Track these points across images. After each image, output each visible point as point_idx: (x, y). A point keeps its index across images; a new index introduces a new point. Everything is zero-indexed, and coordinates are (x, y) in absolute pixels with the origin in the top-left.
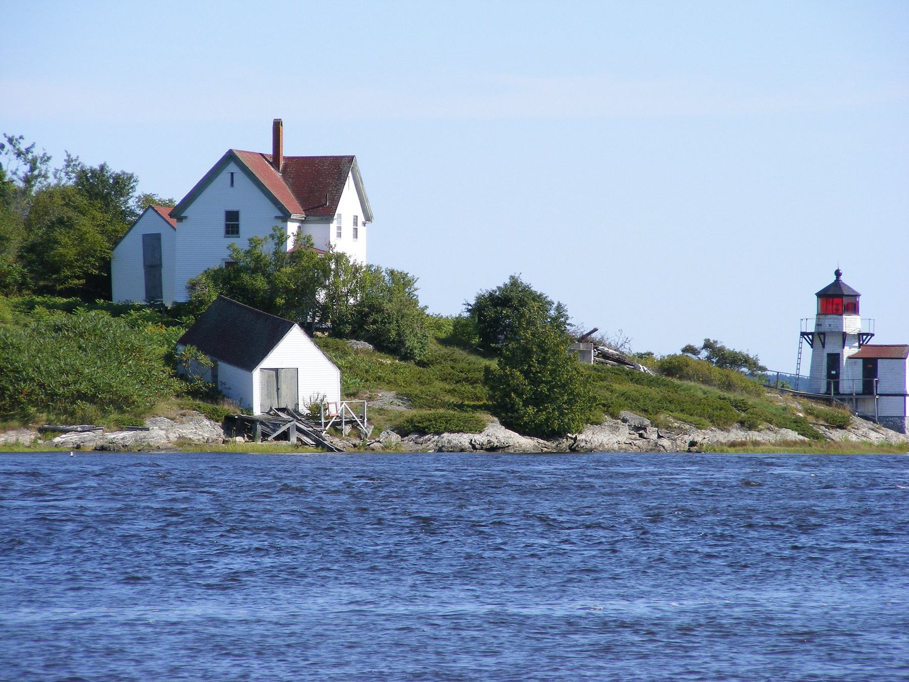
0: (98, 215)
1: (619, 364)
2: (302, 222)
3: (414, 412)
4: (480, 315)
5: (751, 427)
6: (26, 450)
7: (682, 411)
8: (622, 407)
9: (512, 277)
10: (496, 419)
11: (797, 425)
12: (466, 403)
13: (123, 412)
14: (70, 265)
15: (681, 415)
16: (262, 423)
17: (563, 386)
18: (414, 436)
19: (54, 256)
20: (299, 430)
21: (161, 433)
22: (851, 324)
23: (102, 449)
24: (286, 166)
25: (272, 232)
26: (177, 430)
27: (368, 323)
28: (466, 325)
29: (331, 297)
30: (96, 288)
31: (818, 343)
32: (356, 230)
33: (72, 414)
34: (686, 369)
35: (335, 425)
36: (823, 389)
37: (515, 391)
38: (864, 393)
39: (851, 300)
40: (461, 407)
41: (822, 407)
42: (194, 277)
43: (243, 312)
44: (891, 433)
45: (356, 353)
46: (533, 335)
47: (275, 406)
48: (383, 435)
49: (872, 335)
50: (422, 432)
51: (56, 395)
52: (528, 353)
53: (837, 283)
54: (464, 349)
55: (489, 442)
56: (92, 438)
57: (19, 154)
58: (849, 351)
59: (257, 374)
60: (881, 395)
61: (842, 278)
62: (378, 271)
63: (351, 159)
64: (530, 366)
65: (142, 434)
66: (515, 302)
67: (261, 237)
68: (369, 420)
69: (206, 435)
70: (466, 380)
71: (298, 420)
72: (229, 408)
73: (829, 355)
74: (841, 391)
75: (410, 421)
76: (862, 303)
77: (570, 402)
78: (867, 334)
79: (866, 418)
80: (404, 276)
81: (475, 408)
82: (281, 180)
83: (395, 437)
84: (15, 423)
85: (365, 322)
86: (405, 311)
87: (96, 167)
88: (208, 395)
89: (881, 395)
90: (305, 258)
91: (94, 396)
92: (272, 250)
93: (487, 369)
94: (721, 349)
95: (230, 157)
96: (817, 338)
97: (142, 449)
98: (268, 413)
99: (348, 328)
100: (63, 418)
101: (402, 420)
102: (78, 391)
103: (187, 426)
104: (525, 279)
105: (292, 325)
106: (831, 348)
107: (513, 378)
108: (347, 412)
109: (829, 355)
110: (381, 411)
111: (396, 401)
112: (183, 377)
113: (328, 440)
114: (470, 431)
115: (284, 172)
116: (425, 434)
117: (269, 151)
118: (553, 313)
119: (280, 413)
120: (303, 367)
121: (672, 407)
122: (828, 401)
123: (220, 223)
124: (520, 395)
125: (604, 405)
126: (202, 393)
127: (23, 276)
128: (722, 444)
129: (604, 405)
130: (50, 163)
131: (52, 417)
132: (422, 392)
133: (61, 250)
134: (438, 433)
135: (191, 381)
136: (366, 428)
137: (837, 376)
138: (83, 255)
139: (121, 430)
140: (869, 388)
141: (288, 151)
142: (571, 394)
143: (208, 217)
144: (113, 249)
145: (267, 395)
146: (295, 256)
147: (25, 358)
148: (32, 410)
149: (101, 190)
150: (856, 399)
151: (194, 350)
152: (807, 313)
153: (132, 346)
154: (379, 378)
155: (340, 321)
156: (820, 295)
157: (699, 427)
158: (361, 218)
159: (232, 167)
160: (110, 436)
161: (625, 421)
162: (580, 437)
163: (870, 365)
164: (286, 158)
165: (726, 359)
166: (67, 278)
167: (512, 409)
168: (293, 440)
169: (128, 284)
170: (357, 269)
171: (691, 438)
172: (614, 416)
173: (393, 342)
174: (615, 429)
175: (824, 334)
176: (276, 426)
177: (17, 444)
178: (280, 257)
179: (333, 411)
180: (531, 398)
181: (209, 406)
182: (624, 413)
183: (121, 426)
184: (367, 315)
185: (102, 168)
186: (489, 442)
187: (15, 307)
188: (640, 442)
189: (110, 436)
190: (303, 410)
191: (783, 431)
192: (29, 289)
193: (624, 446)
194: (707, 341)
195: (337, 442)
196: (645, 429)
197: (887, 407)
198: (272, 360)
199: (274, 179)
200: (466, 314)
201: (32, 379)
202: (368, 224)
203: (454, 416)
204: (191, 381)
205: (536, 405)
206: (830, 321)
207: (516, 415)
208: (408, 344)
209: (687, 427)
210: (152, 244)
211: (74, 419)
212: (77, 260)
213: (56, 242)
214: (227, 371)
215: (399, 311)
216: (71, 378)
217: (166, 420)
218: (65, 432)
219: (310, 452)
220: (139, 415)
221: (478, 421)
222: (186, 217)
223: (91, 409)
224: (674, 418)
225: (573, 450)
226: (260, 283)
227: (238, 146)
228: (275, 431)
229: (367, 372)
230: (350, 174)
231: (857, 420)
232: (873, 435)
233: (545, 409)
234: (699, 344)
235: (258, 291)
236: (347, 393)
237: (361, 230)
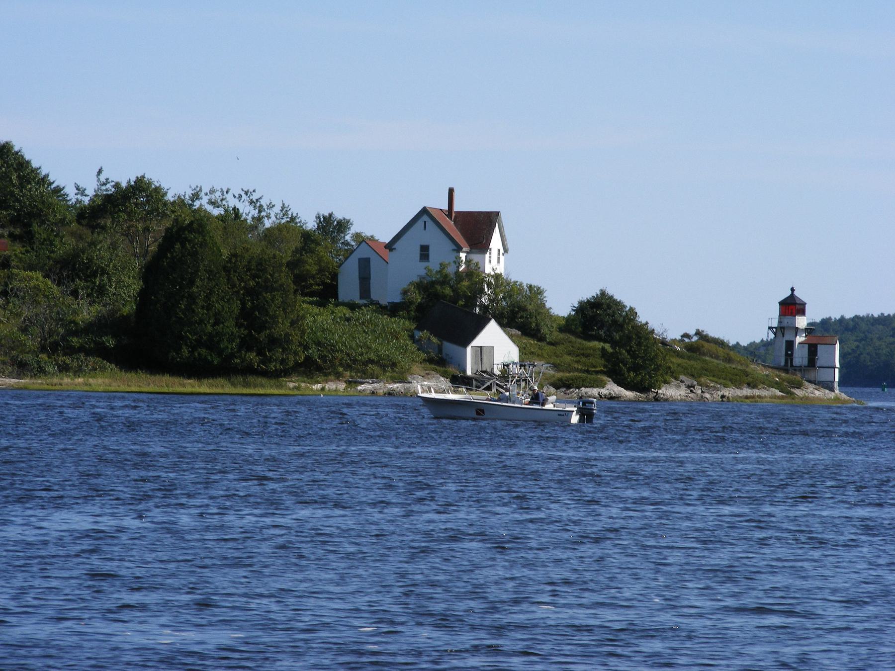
4: (583, 313)
8: (680, 373)
11: (777, 385)
14: (313, 277)
15: (715, 379)
17: (652, 360)
18: (563, 390)
20: (497, 384)
28: (573, 320)
36: (783, 363)
40: (587, 371)
43: (446, 310)
44: (827, 391)
46: (633, 327)
50: (568, 387)
51: (357, 360)
52: (629, 339)
57: (251, 202)
58: (799, 339)
62: (521, 284)
64: (631, 347)
65: (408, 385)
66: (605, 306)
67: (447, 262)
70: (583, 354)
72: (452, 370)
73: (787, 342)
74: (794, 364)
75: (560, 380)
76: (808, 309)
79: (810, 382)
81: (597, 372)
84: (332, 377)
87: (327, 214)
88: (442, 363)
93: (603, 349)
94: (706, 336)
95: (424, 211)
104: (610, 291)
106: (788, 337)
109: (787, 342)
114: (597, 386)
115: (455, 222)
117: (445, 207)
120: (497, 344)
122: (786, 371)
123: (432, 253)
124: (625, 365)
130: (274, 209)
131: (353, 374)
133: (308, 267)
134: (579, 388)
137: (792, 354)
138: (321, 271)
139: (395, 383)
141: (457, 208)
143: (410, 248)
145: (474, 362)
148: (341, 369)
152: (773, 315)
154: (532, 353)
157: (726, 386)
158: (502, 251)
159: (425, 218)
161: (682, 382)
162: (660, 391)
166: (311, 285)
168: (494, 390)
169: (349, 289)
172: (676, 378)
174: (678, 387)
175: (784, 328)
176: (483, 383)
181: (442, 369)
182: (682, 377)
183: (394, 380)
184: (517, 312)
185: (330, 215)
188: (691, 395)
190: (497, 372)
194: (698, 330)
197: (823, 375)
198: (478, 341)
199: (449, 225)
200: (573, 313)
205: (635, 371)
206: (787, 320)
210: (365, 264)
213: (306, 262)
214: (450, 348)
218: (362, 383)
220: (402, 373)
221: (602, 381)
223: (376, 369)
226: (448, 291)
231: (806, 383)
234: (692, 332)
237: (502, 258)
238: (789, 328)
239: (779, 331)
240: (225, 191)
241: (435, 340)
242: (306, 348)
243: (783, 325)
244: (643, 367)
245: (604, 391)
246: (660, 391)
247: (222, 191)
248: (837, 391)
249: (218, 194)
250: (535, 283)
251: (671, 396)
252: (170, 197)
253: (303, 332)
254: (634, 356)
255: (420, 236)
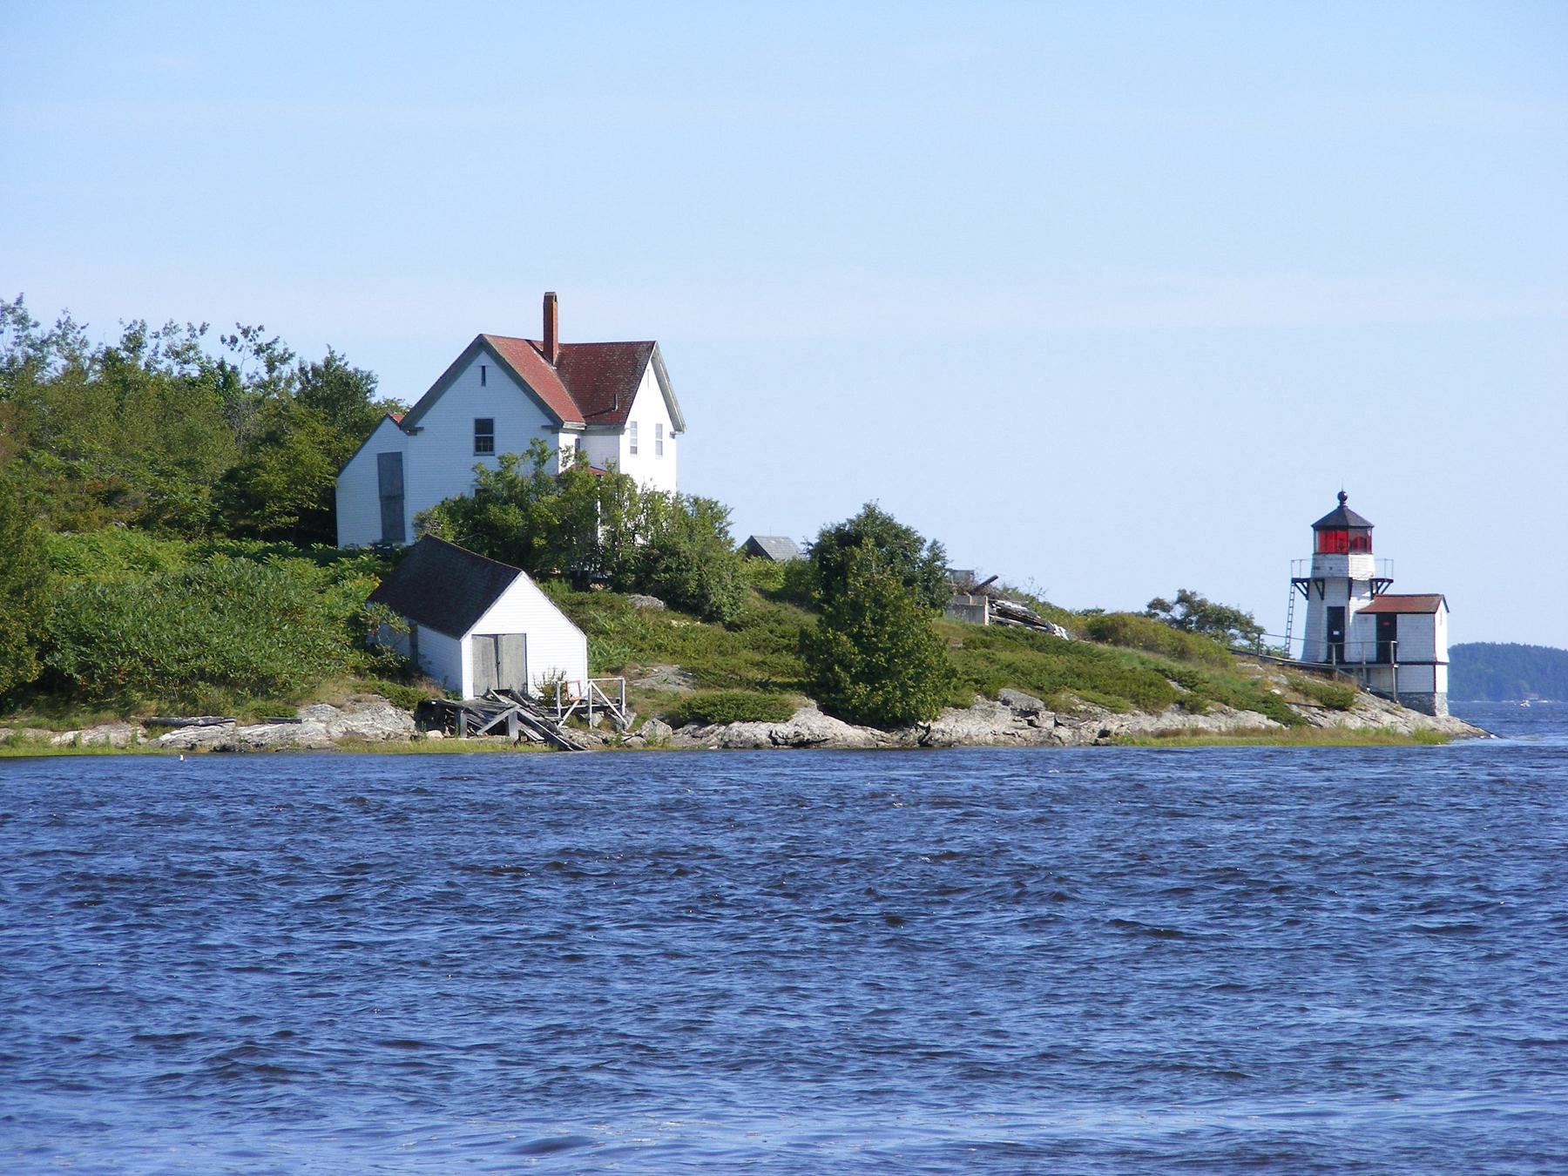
0: (321, 429)
1: (1026, 623)
2: (582, 433)
3: (703, 693)
4: (823, 558)
5: (1193, 708)
6: (120, 752)
7: (1094, 688)
9: (867, 506)
10: (813, 702)
11: (1269, 705)
12: (774, 679)
13: (270, 698)
14: (278, 497)
15: (1092, 694)
16: (468, 711)
18: (690, 727)
19: (256, 485)
21: (317, 726)
22: (1360, 566)
23: (224, 749)
24: (561, 357)
25: (530, 447)
26: (353, 722)
27: (634, 568)
28: (800, 573)
29: (613, 537)
30: (314, 529)
31: (1315, 593)
32: (660, 444)
33: (194, 701)
34: (1122, 631)
35: (577, 712)
36: (1322, 657)
37: (841, 663)
38: (1378, 662)
39: (1359, 534)
40: (764, 685)
41: (1319, 682)
42: (422, 510)
45: (640, 612)
47: (494, 687)
48: (647, 725)
49: (1391, 581)
50: (703, 721)
52: (857, 609)
54: (800, 606)
55: (797, 734)
56: (215, 734)
58: (1357, 603)
59: (467, 642)
60: (1401, 663)
61: (1347, 503)
63: (651, 345)
64: (861, 627)
67: (518, 454)
68: (629, 705)
69: (388, 729)
71: (525, 706)
72: (427, 691)
73: (1330, 609)
74: (1347, 658)
77: (917, 678)
78: (1383, 580)
80: (711, 505)
81: (784, 687)
82: (555, 375)
83: (663, 730)
84: (110, 715)
85: (654, 570)
86: (710, 554)
88: (405, 672)
89: (1401, 663)
90: (578, 483)
91: (224, 676)
92: (531, 473)
94: (1202, 603)
95: (480, 345)
96: (1314, 586)
97: (290, 750)
98: (484, 697)
99: (631, 579)
100: (180, 706)
101: (676, 704)
102: (202, 670)
103: (359, 716)
104: (885, 509)
105: (517, 574)
106: (1333, 599)
107: (838, 644)
108: (595, 694)
109: (1330, 609)
110: (650, 693)
111: (674, 678)
112: (371, 649)
113: (564, 732)
115: (559, 365)
116: (708, 724)
117: (538, 336)
118: (924, 554)
119: (500, 697)
120: (531, 632)
121: (1080, 683)
122: (1328, 673)
124: (846, 668)
125: (977, 681)
126: (391, 670)
127: (215, 514)
128: (1146, 733)
129: (977, 681)
132: (715, 666)
134: (726, 723)
135: (380, 653)
136: (626, 718)
137: (1341, 638)
139: (262, 723)
140: (1384, 655)
141: (566, 334)
142: (919, 665)
144: (337, 475)
145: (482, 672)
146: (565, 480)
147: (127, 623)
149: (336, 394)
150: (1368, 670)
151: (384, 609)
152: (1301, 552)
153: (290, 604)
154: (659, 647)
155: (623, 567)
156: (1316, 527)
157: (1115, 709)
158: (668, 427)
159: (483, 359)
160: (244, 731)
161: (1006, 702)
162: (934, 726)
163: (1386, 624)
164: (567, 347)
165: (1220, 619)
166: (273, 514)
167: (837, 687)
168: (514, 735)
169: (359, 521)
170: (653, 499)
171: (1101, 726)
173: (693, 596)
174: (989, 714)
175: (1323, 580)
177: (106, 744)
178: (541, 485)
179: (573, 691)
180: (863, 672)
181: (398, 688)
183: (262, 717)
184: (656, 560)
186: (797, 734)
187: (188, 554)
188: (1028, 733)
189: (244, 731)
190: (535, 692)
191: (1242, 714)
192: (222, 530)
193: (1002, 738)
195: (579, 736)
196: (1036, 714)
197: (1411, 680)
199: (547, 379)
201: (134, 653)
202: (679, 435)
203: (749, 698)
204: (377, 653)
205: (870, 681)
206: (1331, 562)
207: (841, 696)
208: (713, 599)
209: (1098, 710)
210: (391, 466)
211: (195, 709)
212: (289, 490)
213: (260, 465)
214: (430, 639)
215: (701, 554)
216: (190, 652)
217: (330, 708)
218: (180, 726)
219: (539, 752)
220: (294, 703)
221: (784, 705)
222: (421, 429)
223: (217, 694)
224: (1081, 698)
225: (924, 744)
226: (514, 517)
227: (494, 328)
228: (486, 722)
229: (643, 638)
230: (650, 366)
231: (1365, 698)
232: (1387, 719)
233: (882, 687)
234: (1170, 597)
235: (510, 528)
236: (599, 665)
238: (1334, 579)
239: (1313, 587)
240: (198, 327)
241: (399, 623)
242: (46, 648)
243: (1323, 573)
244: (888, 672)
245: (784, 729)
246: (934, 726)
247: (191, 329)
248: (1443, 711)
249: (185, 335)
250: (705, 494)
251: (968, 736)
252: (399, 382)
253: (40, 614)
254: (868, 649)
255: (470, 401)
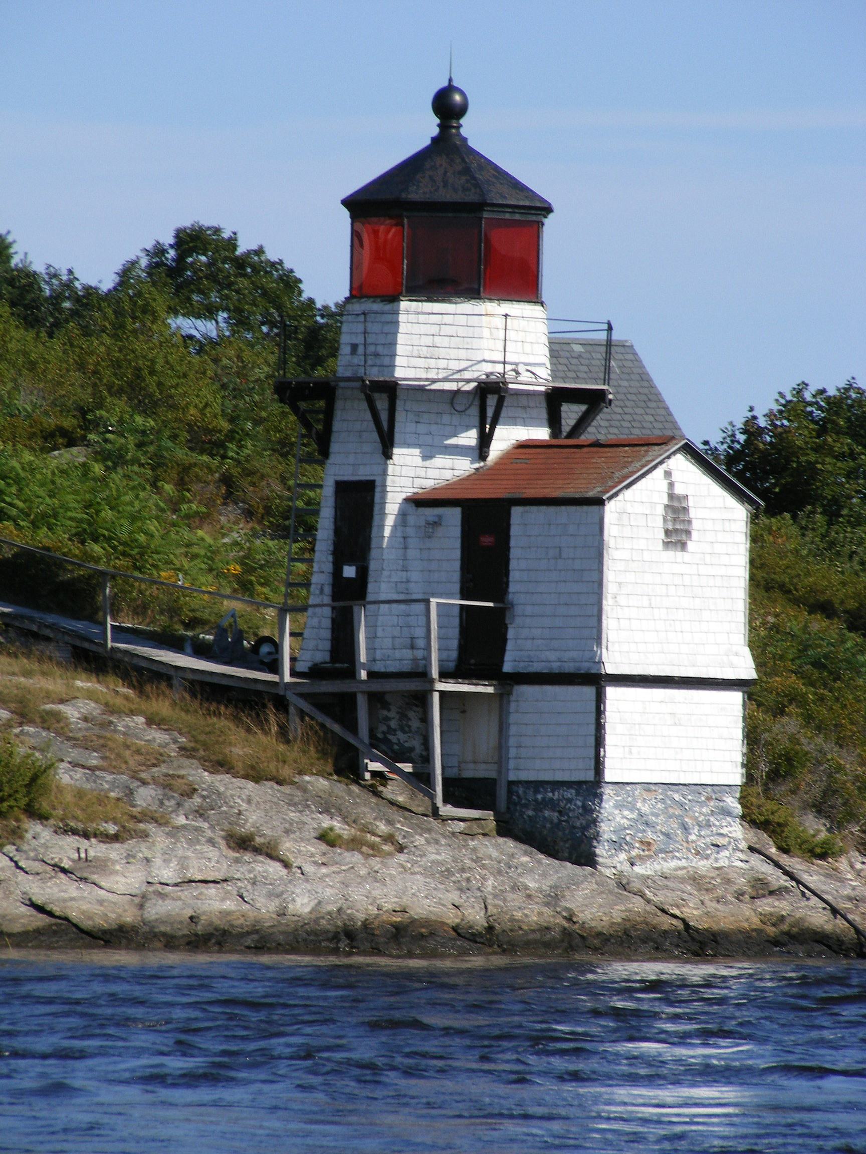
53: (448, 143)
58: (410, 472)
73: (342, 487)
109: (342, 487)
156: (359, 205)
